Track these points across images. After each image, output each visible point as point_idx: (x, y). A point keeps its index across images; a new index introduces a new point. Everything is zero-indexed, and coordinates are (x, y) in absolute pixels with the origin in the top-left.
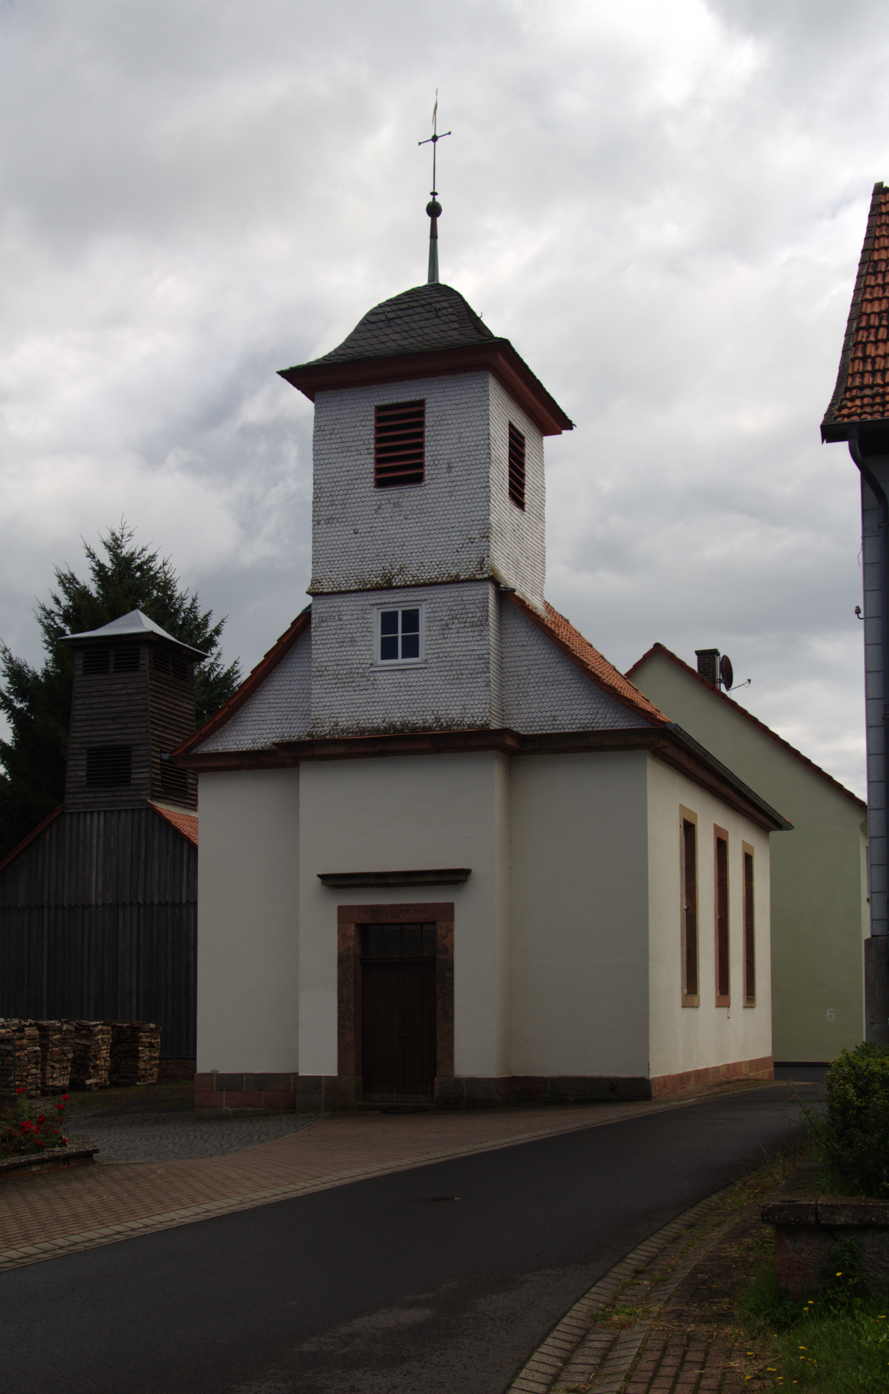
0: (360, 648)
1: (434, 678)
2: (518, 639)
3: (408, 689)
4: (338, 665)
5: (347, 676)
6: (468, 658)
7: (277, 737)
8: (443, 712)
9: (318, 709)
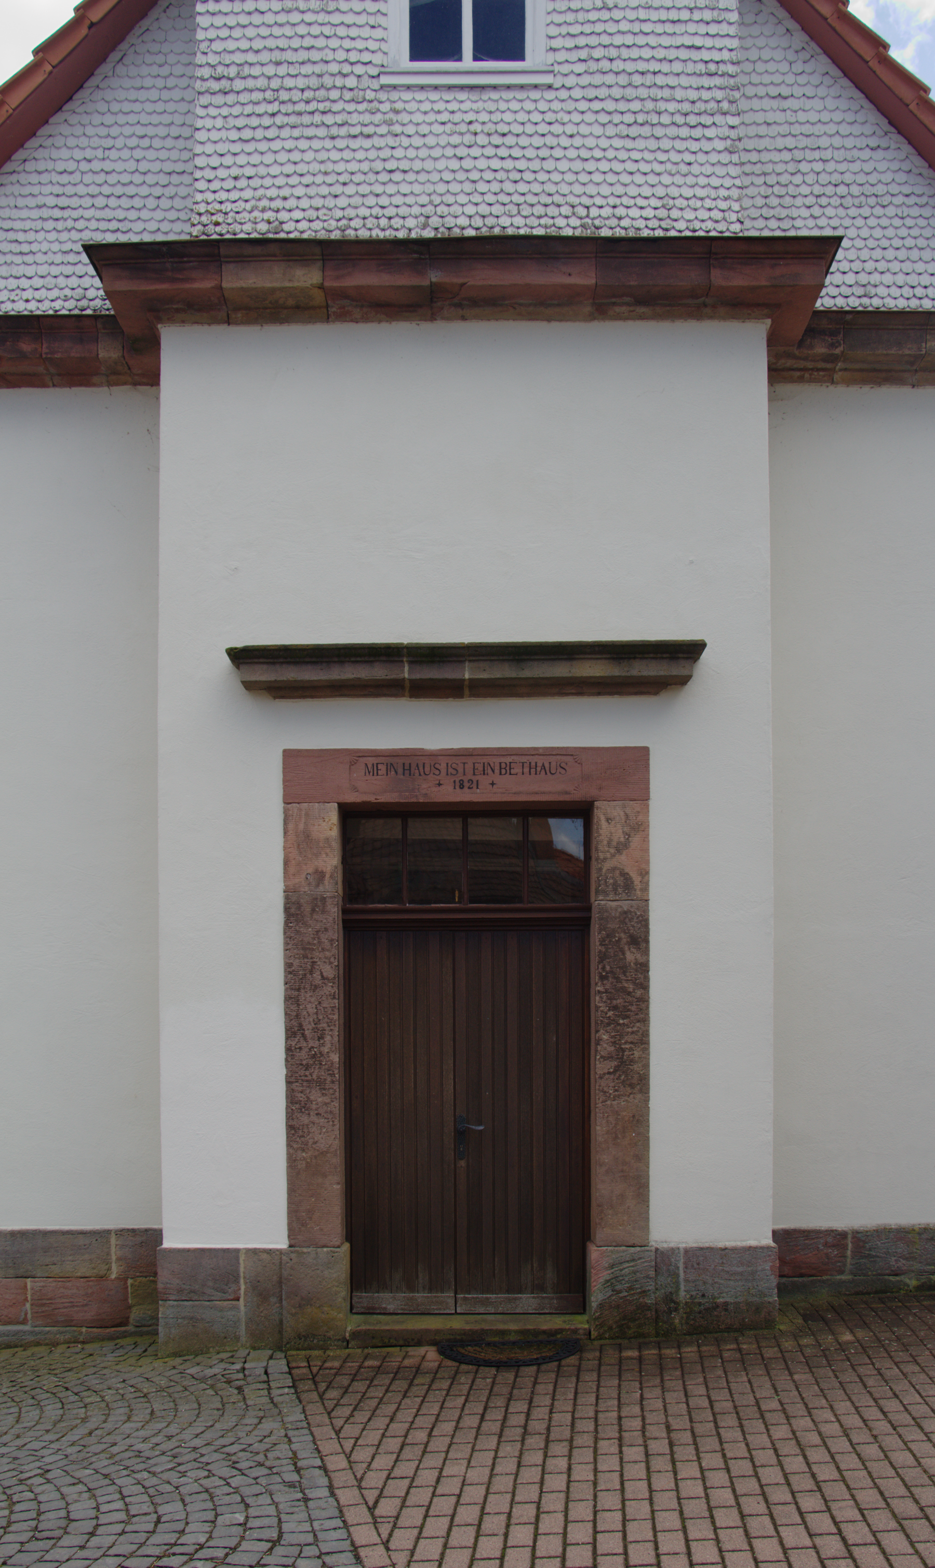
0: (349, 19)
1: (576, 118)
2: (766, 79)
3: (496, 140)
4: (278, 64)
5: (308, 94)
6: (677, 67)
7: (66, 299)
8: (607, 212)
9: (215, 185)
